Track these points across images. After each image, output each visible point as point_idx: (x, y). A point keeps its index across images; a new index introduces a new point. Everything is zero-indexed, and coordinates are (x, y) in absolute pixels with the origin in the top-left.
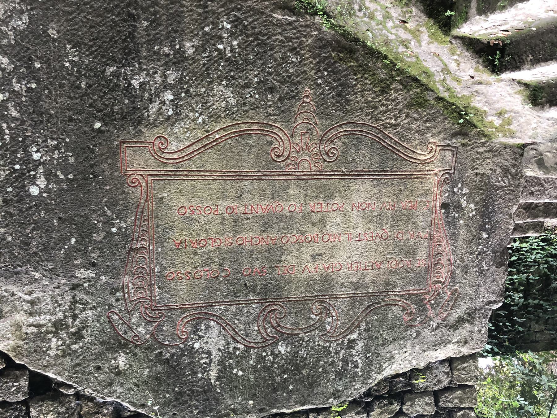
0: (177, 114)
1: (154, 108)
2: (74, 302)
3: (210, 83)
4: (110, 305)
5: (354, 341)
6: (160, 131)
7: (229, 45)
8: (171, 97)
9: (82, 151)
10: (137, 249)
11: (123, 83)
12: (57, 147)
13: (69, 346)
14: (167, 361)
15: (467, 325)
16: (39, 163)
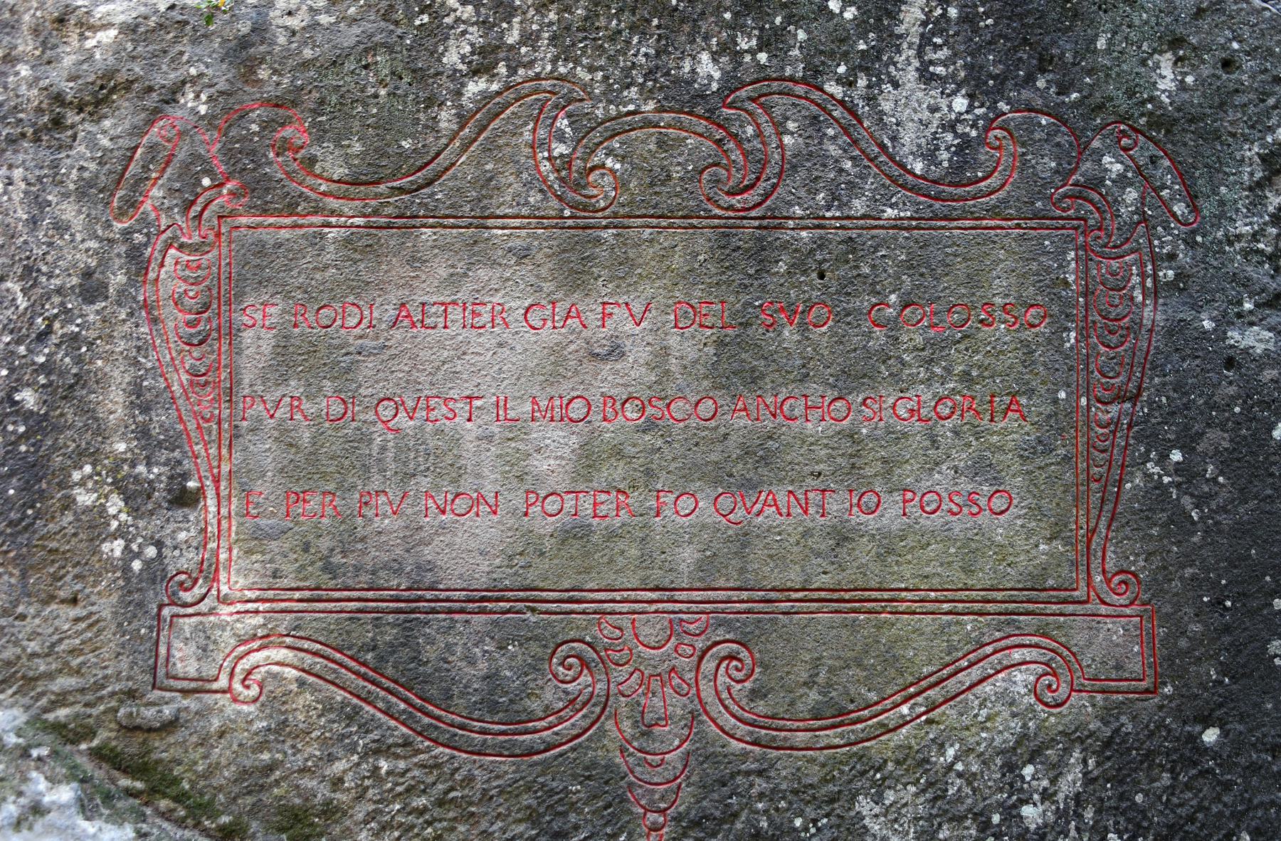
1: (1071, 782)
4: (1191, 244)
8: (1027, 811)
10: (1119, 398)
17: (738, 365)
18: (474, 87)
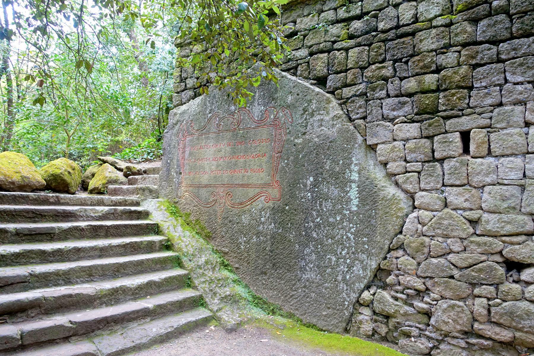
0: (260, 212)
1: (268, 215)
2: (306, 126)
3: (249, 224)
4: (292, 126)
5: (210, 113)
6: (267, 205)
7: (242, 239)
8: (262, 219)
9: (293, 196)
10: (279, 153)
11: (277, 225)
12: (302, 198)
13: (309, 105)
14: (273, 99)
15: (174, 122)
16: (309, 191)
17: (234, 152)
18: (209, 115)
